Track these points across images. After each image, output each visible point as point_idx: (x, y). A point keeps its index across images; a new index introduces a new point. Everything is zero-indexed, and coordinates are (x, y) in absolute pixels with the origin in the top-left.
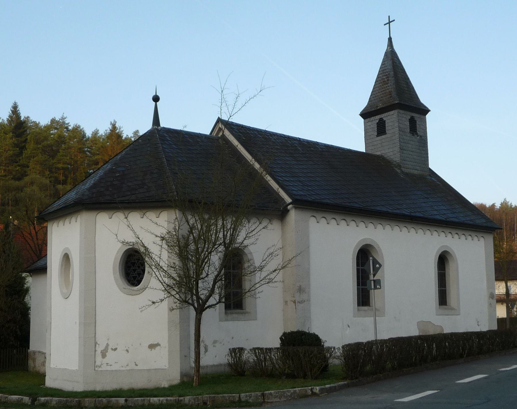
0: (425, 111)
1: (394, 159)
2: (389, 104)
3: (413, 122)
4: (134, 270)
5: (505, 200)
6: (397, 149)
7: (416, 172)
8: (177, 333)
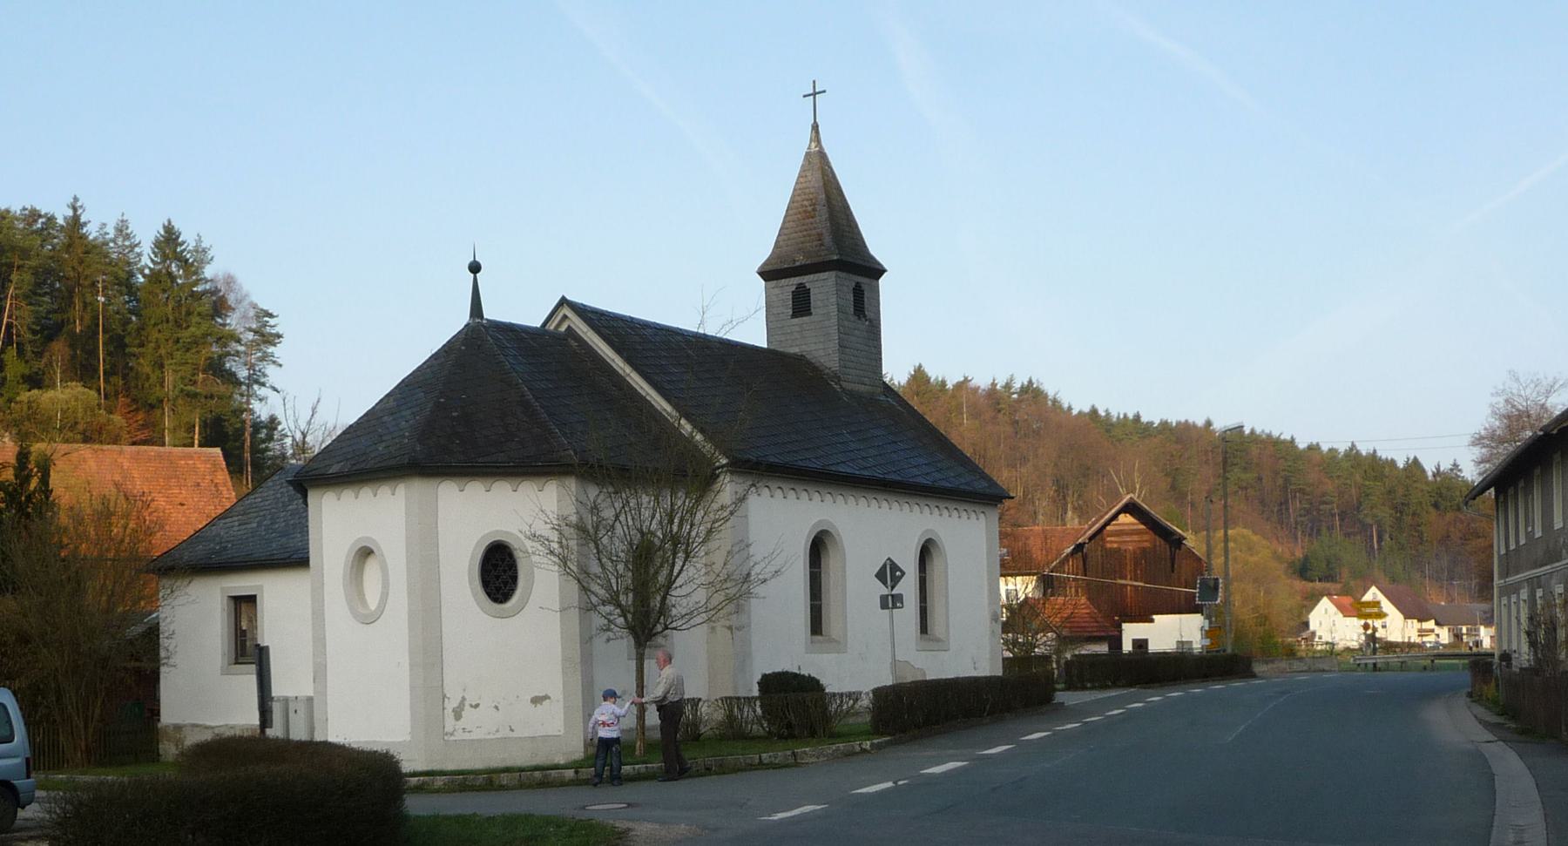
0: (877, 271)
1: (828, 364)
2: (820, 259)
3: (858, 292)
4: (498, 577)
6: (833, 345)
7: (862, 388)
8: (577, 679)
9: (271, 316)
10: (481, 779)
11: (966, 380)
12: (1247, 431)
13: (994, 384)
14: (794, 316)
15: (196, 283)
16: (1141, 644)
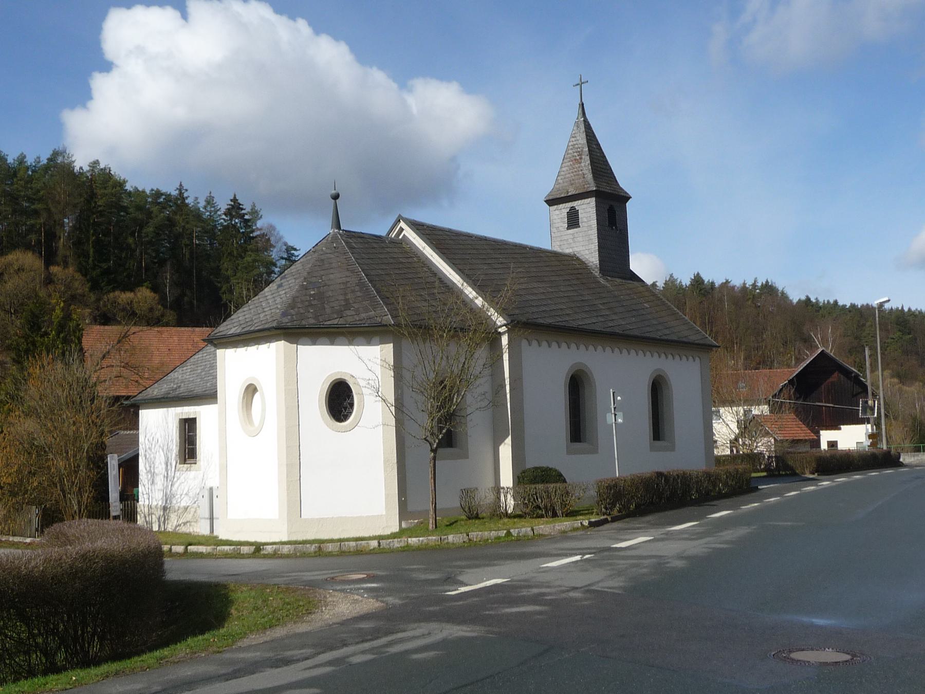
1: (591, 260)
2: (584, 191)
5: (671, 276)
9: (295, 250)
10: (313, 548)
11: (727, 282)
12: (906, 309)
13: (744, 284)
14: (568, 228)
15: (253, 231)
16: (833, 444)
